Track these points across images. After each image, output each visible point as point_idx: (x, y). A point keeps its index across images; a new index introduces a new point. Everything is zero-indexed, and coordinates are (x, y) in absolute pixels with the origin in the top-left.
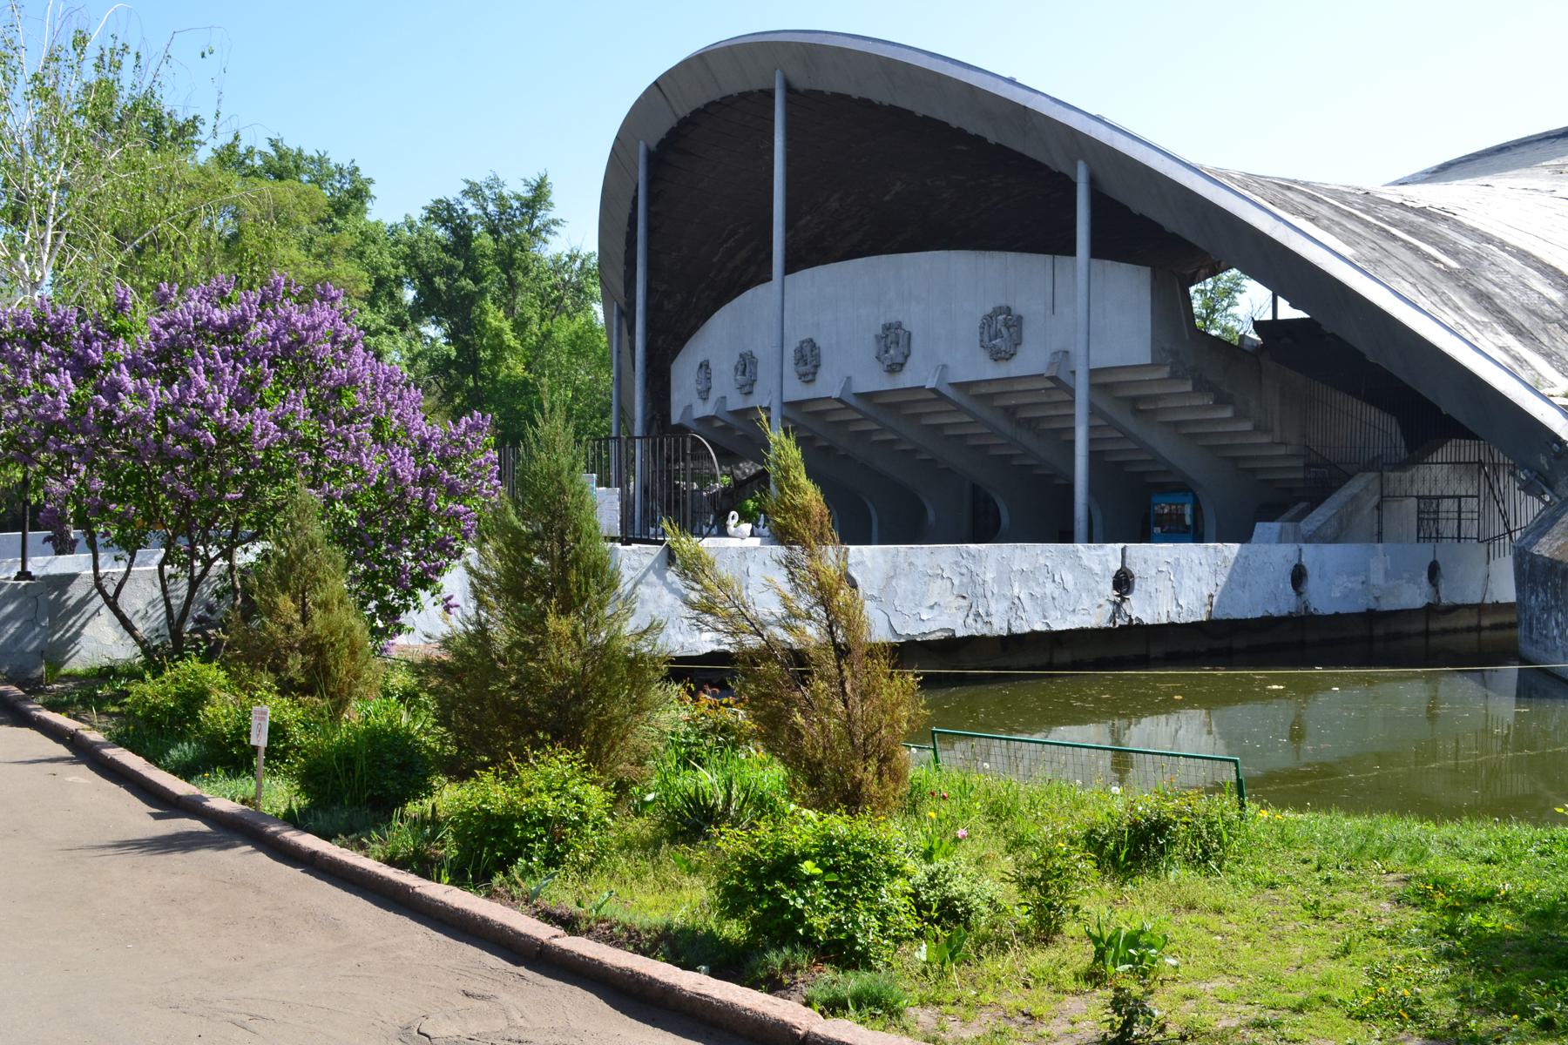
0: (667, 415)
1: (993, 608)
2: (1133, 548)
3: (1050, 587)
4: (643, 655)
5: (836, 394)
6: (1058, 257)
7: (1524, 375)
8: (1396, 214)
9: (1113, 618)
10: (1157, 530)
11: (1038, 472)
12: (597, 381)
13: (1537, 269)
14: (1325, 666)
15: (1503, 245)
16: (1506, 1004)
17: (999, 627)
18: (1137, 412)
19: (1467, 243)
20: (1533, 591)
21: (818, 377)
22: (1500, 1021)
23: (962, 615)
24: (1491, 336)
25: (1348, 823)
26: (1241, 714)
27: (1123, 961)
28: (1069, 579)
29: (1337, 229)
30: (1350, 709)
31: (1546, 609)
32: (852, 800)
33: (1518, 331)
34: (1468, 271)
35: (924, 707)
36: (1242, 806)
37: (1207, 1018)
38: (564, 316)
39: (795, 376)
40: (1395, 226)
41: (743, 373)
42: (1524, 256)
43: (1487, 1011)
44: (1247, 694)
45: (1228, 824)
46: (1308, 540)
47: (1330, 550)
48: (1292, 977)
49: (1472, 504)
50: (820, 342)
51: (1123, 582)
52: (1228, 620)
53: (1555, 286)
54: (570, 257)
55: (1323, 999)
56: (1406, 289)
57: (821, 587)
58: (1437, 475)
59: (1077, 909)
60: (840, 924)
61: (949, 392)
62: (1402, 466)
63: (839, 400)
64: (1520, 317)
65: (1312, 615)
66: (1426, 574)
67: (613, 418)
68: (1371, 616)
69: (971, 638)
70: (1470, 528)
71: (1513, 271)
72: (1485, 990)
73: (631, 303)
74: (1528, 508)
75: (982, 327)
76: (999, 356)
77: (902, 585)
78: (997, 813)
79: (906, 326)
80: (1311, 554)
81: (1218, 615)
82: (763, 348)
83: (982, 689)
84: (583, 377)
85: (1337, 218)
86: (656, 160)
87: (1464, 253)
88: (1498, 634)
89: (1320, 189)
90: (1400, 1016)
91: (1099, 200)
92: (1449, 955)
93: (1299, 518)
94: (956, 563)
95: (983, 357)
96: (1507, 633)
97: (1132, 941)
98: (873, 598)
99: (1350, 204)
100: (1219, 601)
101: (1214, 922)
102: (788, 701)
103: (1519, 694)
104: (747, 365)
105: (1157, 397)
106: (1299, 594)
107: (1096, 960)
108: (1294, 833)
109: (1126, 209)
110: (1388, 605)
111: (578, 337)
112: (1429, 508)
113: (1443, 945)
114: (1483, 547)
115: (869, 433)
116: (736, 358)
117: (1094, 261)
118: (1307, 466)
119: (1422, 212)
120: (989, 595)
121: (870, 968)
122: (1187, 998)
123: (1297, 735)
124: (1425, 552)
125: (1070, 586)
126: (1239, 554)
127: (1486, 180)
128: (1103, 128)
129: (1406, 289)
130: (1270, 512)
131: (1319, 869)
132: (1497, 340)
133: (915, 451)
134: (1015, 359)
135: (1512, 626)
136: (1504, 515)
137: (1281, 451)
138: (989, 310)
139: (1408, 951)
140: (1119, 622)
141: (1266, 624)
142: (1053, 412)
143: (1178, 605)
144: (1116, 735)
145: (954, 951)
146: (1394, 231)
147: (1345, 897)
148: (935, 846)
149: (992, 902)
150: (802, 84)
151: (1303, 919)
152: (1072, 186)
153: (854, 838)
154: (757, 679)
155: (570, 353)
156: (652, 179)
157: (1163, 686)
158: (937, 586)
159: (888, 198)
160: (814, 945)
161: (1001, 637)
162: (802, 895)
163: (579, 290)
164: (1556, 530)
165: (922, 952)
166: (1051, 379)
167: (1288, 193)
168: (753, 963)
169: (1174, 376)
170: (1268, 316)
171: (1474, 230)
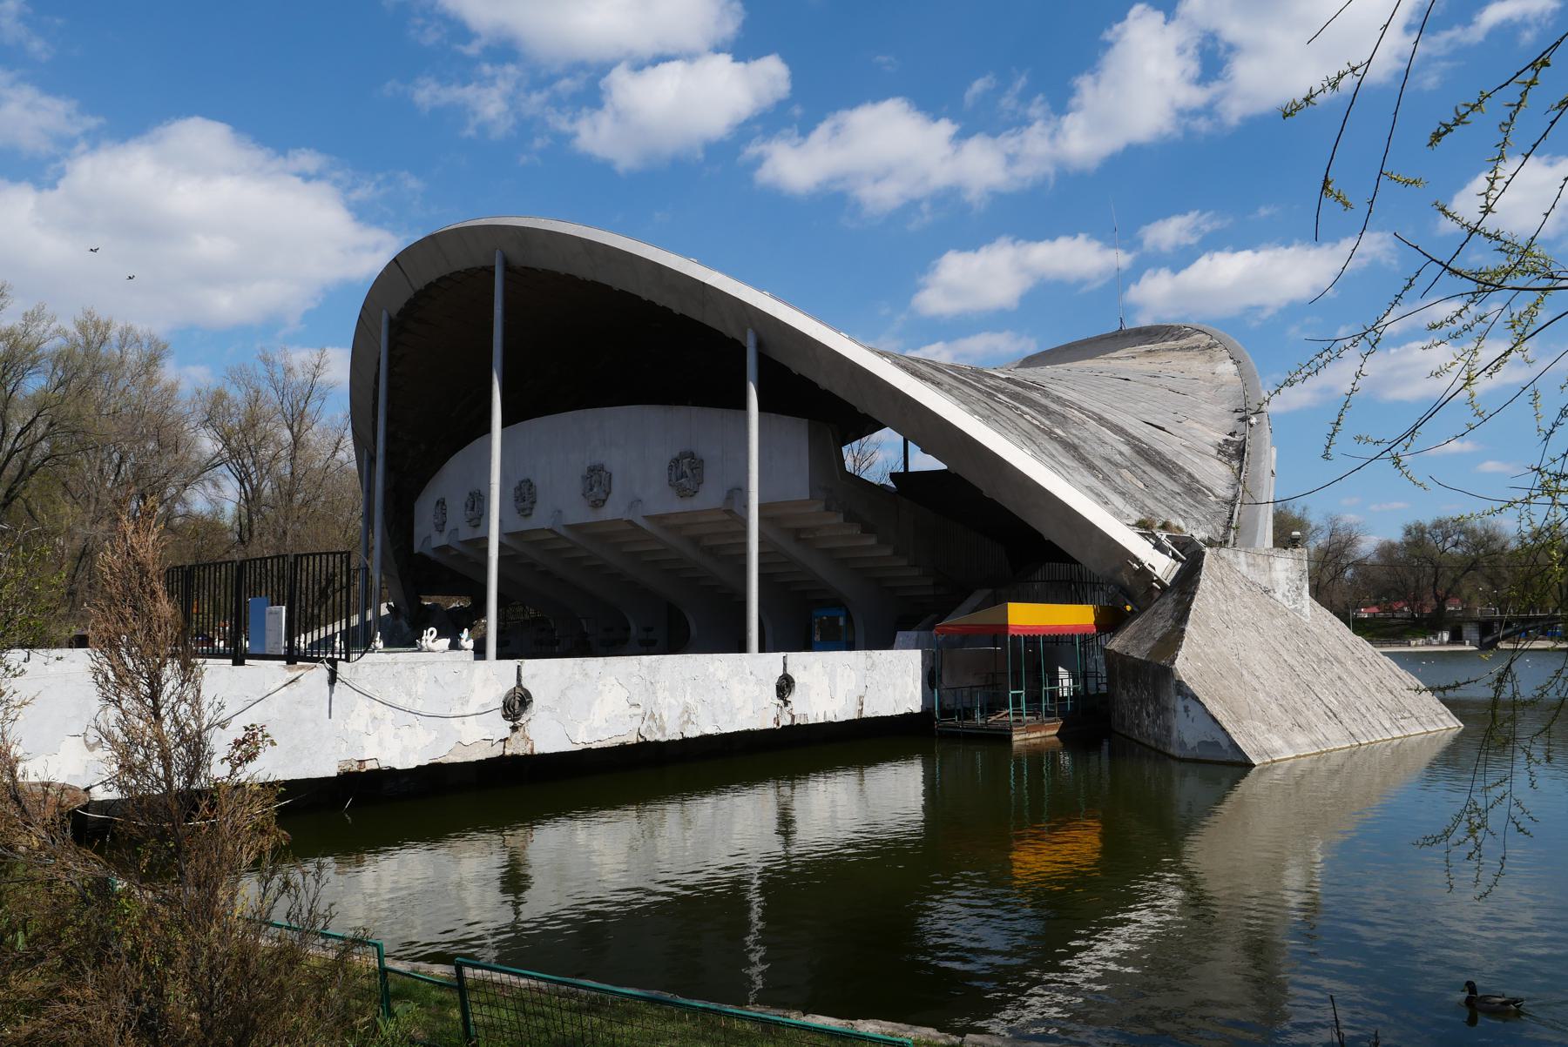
2: (794, 657)
9: (777, 721)
51: (785, 686)
76: (684, 493)
85: (956, 384)
86: (398, 326)
91: (764, 360)
93: (930, 627)
138: (676, 454)
152: (743, 350)
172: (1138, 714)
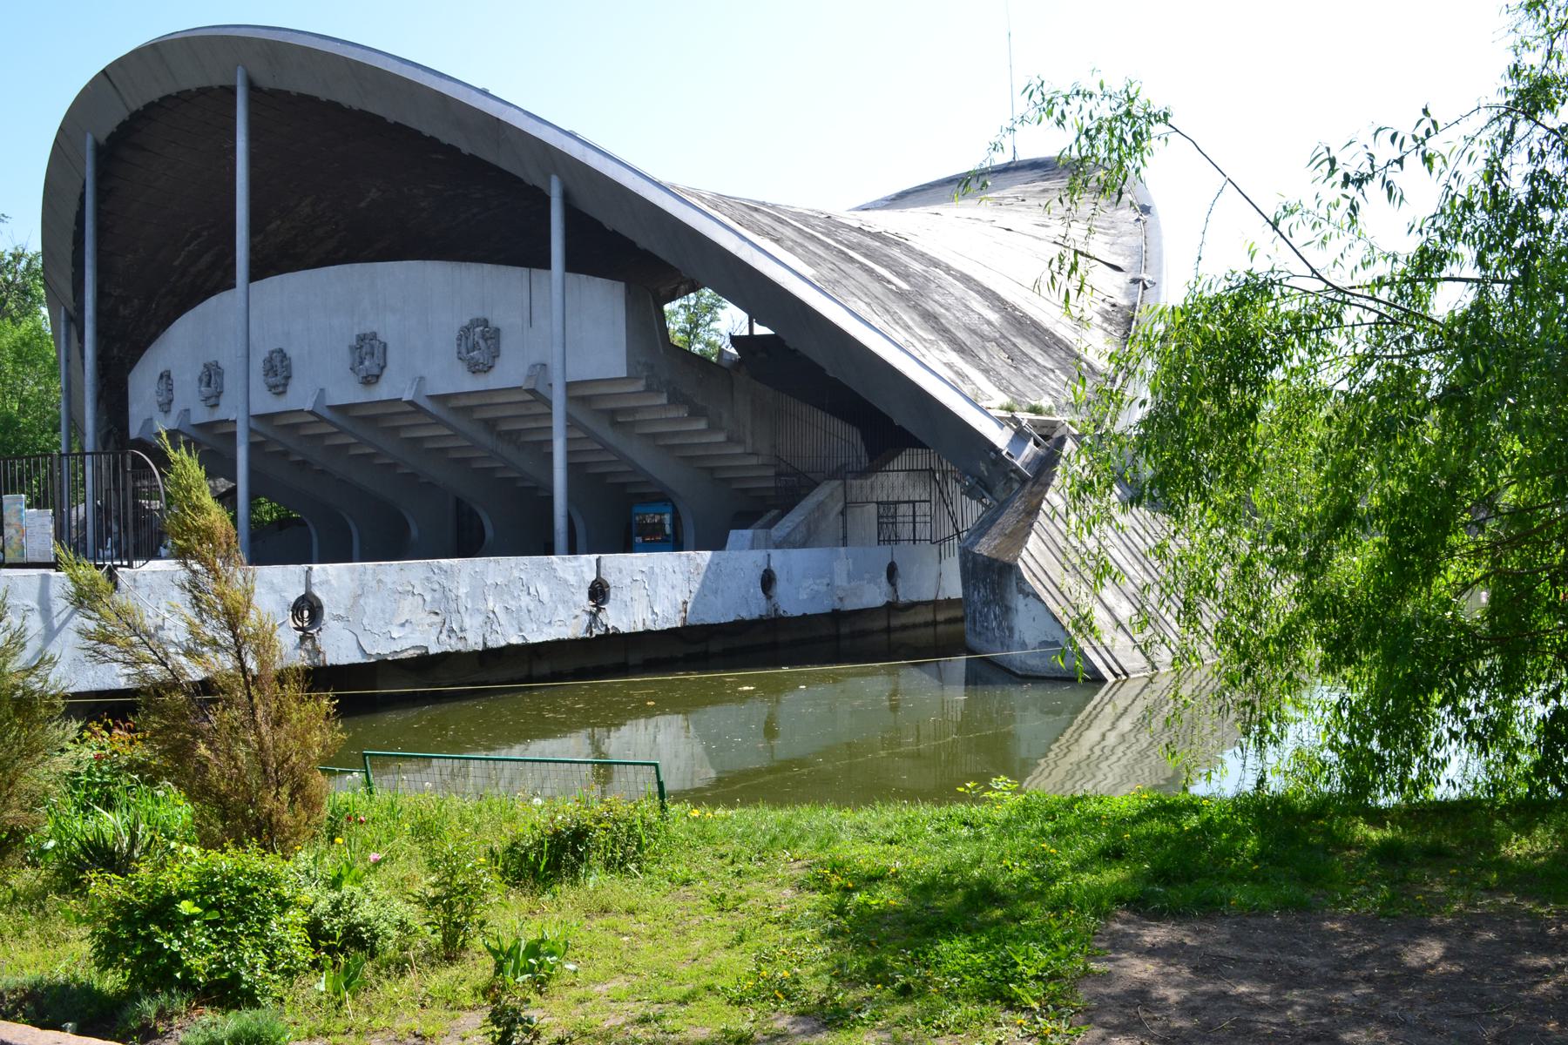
0: (124, 427)
1: (467, 623)
2: (608, 558)
3: (525, 599)
4: (33, 692)
5: (308, 406)
6: (534, 270)
7: (966, 389)
8: (855, 238)
9: (589, 629)
10: (639, 540)
11: (520, 484)
12: (47, 391)
13: (978, 292)
14: (790, 665)
15: (948, 269)
16: (873, 975)
17: (474, 642)
18: (615, 424)
19: (916, 267)
20: (976, 587)
21: (290, 390)
22: (865, 991)
23: (434, 631)
24: (936, 353)
25: (772, 815)
26: (717, 716)
27: (524, 971)
28: (544, 591)
29: (800, 250)
30: (821, 705)
31: (987, 603)
32: (267, 833)
33: (961, 348)
34: (918, 292)
35: (340, 731)
36: (663, 807)
37: (593, 1019)
38: (7, 320)
39: (265, 388)
40: (853, 249)
41: (209, 385)
42: (966, 280)
43: (855, 983)
44: (718, 696)
45: (650, 826)
46: (777, 546)
47: (797, 555)
48: (685, 970)
49: (923, 509)
50: (292, 352)
51: (599, 592)
52: (702, 626)
53: (993, 307)
54: (14, 257)
55: (709, 988)
56: (861, 308)
57: (227, 612)
58: (894, 483)
59: (483, 923)
60: (223, 963)
61: (428, 405)
62: (863, 474)
63: (311, 413)
64: (962, 335)
65: (782, 618)
66: (885, 574)
67: (61, 437)
68: (837, 616)
69: (446, 655)
70: (923, 531)
71: (957, 294)
72: (857, 963)
73: (80, 309)
74: (972, 511)
75: (459, 339)
76: (476, 369)
77: (370, 603)
78: (425, 831)
79: (381, 337)
80: (778, 559)
81: (692, 621)
82: (228, 357)
83: (455, 705)
84: (31, 388)
86: (107, 154)
87: (913, 275)
88: (952, 628)
89: (785, 211)
90: (776, 997)
91: (573, 216)
92: (833, 934)
93: (770, 525)
94: (428, 579)
95: (461, 368)
96: (958, 627)
97: (533, 950)
98: (339, 618)
99: (812, 227)
100: (693, 607)
101: (626, 923)
102: (194, 733)
103: (967, 683)
104: (212, 376)
105: (634, 410)
106: (769, 597)
107: (497, 973)
108: (717, 830)
109: (600, 224)
110: (851, 604)
111: (24, 344)
112: (887, 512)
113: (830, 925)
114: (935, 548)
115: (347, 446)
116: (201, 368)
117: (571, 276)
118: (778, 475)
119: (877, 236)
120: (462, 610)
121: (257, 1005)
122: (580, 1001)
123: (770, 731)
124: (884, 554)
125: (545, 597)
126: (711, 561)
127: (936, 208)
128: (576, 143)
129: (861, 308)
130: (744, 519)
131: (733, 862)
132: (941, 357)
133: (394, 466)
134: (495, 371)
135: (961, 620)
136: (952, 515)
137: (754, 461)
138: (466, 321)
139: (797, 934)
140: (596, 632)
141: (739, 627)
142: (534, 425)
143: (653, 612)
144: (596, 747)
145: (350, 979)
146: (851, 253)
147: (752, 887)
148: (344, 872)
149: (402, 925)
150: (266, 82)
151: (710, 912)
153: (239, 873)
154: (161, 712)
155: (15, 362)
156: (100, 177)
157: (636, 694)
158: (408, 604)
159: (363, 205)
160: (194, 988)
161: (476, 652)
162: (179, 937)
163: (25, 292)
164: (994, 530)
165: (322, 984)
166: (532, 391)
167: (755, 214)
168: (126, 1015)
169: (649, 389)
170: (746, 333)
171: (923, 255)
172: (986, 617)
